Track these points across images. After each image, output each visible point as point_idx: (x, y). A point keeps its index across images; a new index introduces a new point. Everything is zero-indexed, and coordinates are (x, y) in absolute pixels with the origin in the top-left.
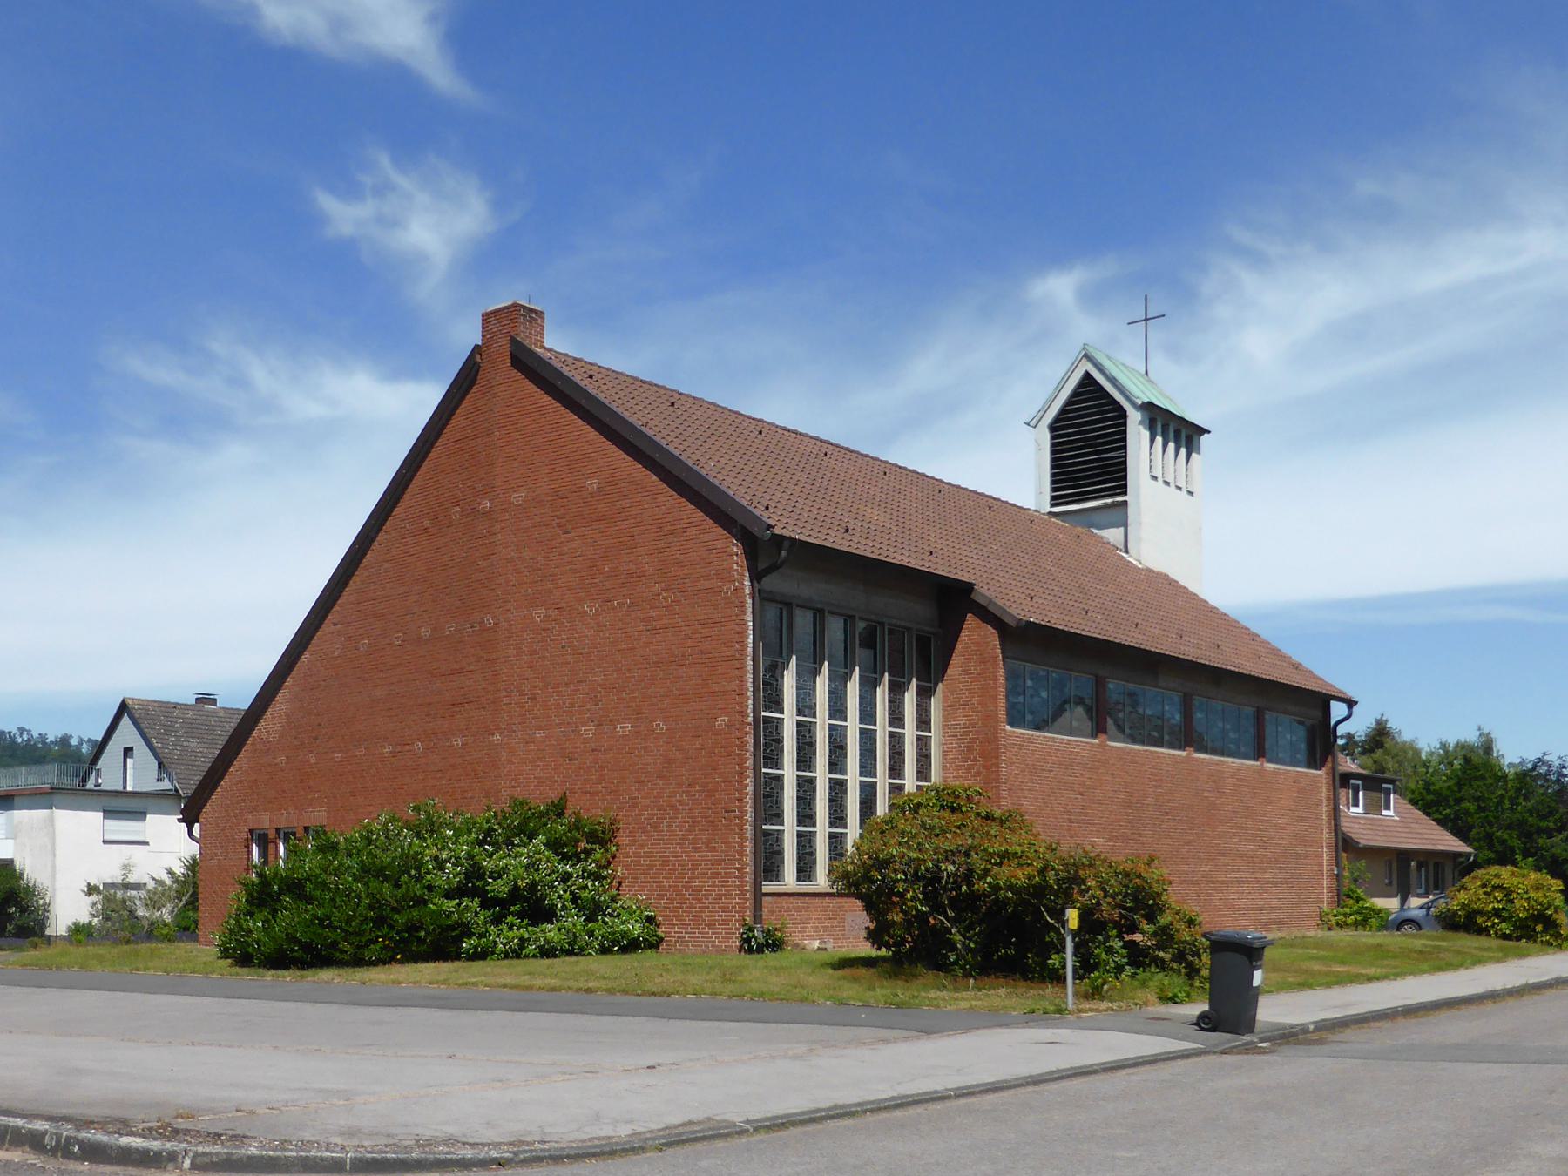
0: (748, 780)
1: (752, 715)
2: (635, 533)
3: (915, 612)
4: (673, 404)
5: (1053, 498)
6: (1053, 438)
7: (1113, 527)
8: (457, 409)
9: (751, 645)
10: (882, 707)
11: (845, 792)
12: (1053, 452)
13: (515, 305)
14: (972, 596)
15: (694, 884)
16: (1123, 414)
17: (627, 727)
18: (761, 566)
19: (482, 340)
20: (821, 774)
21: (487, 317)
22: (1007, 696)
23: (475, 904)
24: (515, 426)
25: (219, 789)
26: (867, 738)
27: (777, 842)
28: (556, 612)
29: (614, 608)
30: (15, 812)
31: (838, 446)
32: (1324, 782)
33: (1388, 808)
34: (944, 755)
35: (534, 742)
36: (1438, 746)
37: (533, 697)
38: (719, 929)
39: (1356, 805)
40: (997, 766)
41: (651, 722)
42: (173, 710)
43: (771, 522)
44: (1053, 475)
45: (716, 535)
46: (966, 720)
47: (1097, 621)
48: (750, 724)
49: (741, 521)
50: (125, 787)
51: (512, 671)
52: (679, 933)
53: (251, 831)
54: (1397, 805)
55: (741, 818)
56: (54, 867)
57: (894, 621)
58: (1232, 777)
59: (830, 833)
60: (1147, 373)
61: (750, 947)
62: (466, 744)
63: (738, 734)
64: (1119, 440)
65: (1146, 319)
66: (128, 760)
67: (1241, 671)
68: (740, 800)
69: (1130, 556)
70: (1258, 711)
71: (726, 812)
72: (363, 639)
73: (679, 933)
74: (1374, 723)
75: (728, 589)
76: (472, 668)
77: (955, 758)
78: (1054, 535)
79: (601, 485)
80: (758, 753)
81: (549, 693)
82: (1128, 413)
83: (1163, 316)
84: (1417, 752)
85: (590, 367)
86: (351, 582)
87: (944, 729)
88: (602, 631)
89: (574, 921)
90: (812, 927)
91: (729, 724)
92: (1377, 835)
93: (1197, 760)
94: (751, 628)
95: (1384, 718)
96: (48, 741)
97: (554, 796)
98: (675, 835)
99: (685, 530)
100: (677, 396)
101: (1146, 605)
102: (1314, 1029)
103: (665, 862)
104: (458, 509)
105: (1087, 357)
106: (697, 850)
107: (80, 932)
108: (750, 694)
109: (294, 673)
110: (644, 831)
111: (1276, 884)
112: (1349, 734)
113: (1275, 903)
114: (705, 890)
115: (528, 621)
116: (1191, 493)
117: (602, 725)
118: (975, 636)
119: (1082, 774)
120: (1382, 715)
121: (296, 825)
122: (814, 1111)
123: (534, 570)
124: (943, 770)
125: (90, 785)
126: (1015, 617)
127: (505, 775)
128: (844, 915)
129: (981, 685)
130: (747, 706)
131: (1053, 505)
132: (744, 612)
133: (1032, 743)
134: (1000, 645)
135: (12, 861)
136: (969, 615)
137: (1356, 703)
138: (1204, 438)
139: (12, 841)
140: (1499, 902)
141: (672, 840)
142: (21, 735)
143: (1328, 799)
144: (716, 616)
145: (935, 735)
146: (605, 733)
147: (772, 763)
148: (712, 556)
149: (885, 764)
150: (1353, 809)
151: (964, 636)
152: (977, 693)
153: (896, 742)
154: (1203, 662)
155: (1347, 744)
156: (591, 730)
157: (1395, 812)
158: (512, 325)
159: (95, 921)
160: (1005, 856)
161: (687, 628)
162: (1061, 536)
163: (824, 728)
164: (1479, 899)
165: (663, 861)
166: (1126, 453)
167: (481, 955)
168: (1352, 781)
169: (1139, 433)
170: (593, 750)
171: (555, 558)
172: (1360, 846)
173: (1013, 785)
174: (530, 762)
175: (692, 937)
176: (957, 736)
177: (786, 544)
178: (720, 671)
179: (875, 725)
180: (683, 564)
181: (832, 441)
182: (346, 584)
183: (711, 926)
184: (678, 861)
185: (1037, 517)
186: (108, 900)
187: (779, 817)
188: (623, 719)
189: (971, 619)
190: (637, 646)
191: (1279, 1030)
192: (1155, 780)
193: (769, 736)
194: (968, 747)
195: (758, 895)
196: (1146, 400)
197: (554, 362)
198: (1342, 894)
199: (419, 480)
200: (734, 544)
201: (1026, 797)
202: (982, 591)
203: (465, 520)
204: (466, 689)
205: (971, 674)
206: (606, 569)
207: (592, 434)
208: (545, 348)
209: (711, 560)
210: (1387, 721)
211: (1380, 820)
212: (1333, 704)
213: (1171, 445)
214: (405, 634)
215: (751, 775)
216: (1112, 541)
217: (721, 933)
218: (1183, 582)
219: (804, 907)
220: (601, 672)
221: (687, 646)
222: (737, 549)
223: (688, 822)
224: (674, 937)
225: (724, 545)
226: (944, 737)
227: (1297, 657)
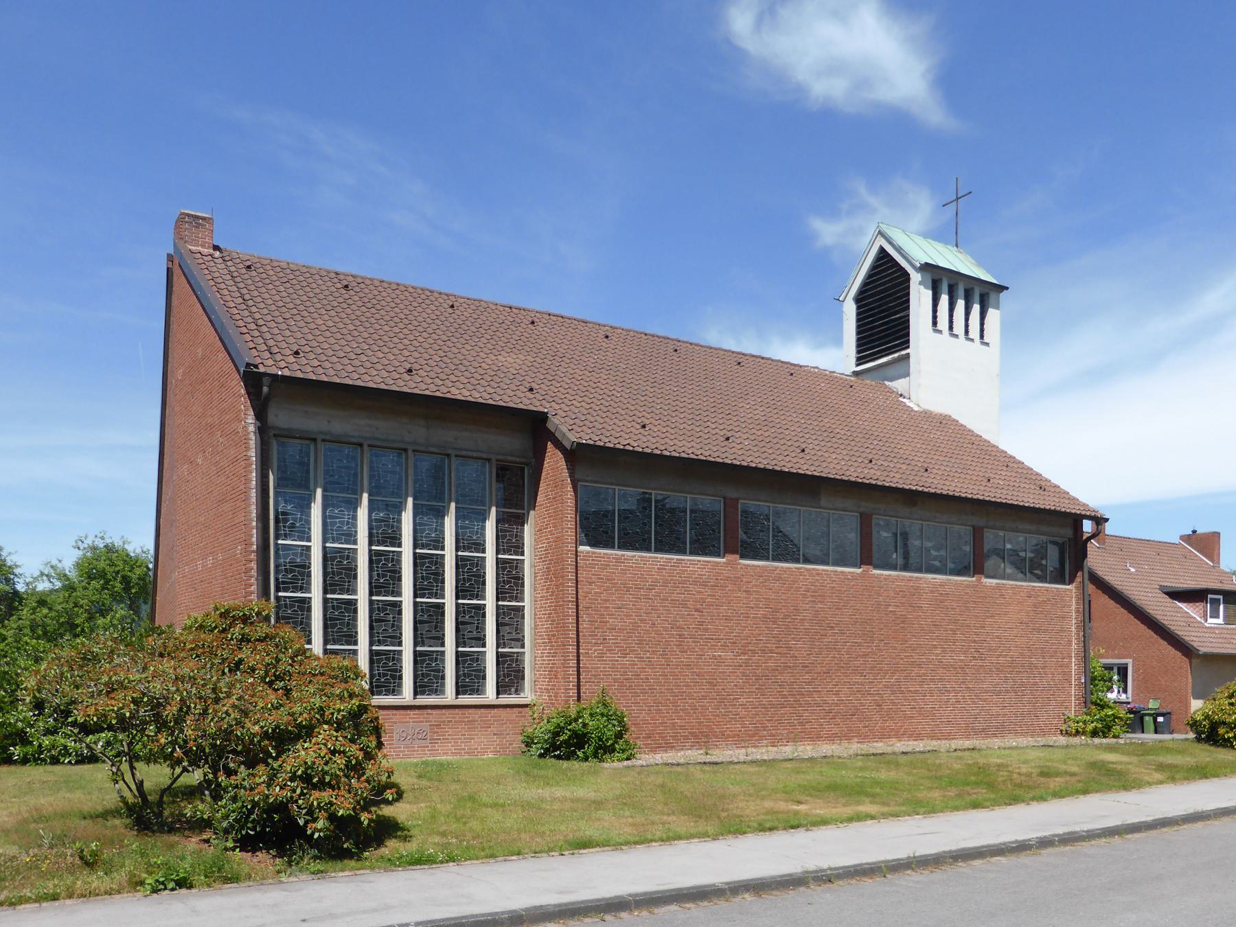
4: (739, 363)
5: (858, 359)
6: (858, 308)
44: (858, 340)
48: (253, 552)
58: (932, 592)
65: (958, 199)
93: (878, 577)
100: (351, 279)
105: (881, 233)
113: (995, 710)
131: (857, 365)
132: (247, 449)
137: (1107, 520)
143: (1077, 611)
151: (547, 460)
168: (1210, 596)
198: (1088, 702)
201: (612, 615)
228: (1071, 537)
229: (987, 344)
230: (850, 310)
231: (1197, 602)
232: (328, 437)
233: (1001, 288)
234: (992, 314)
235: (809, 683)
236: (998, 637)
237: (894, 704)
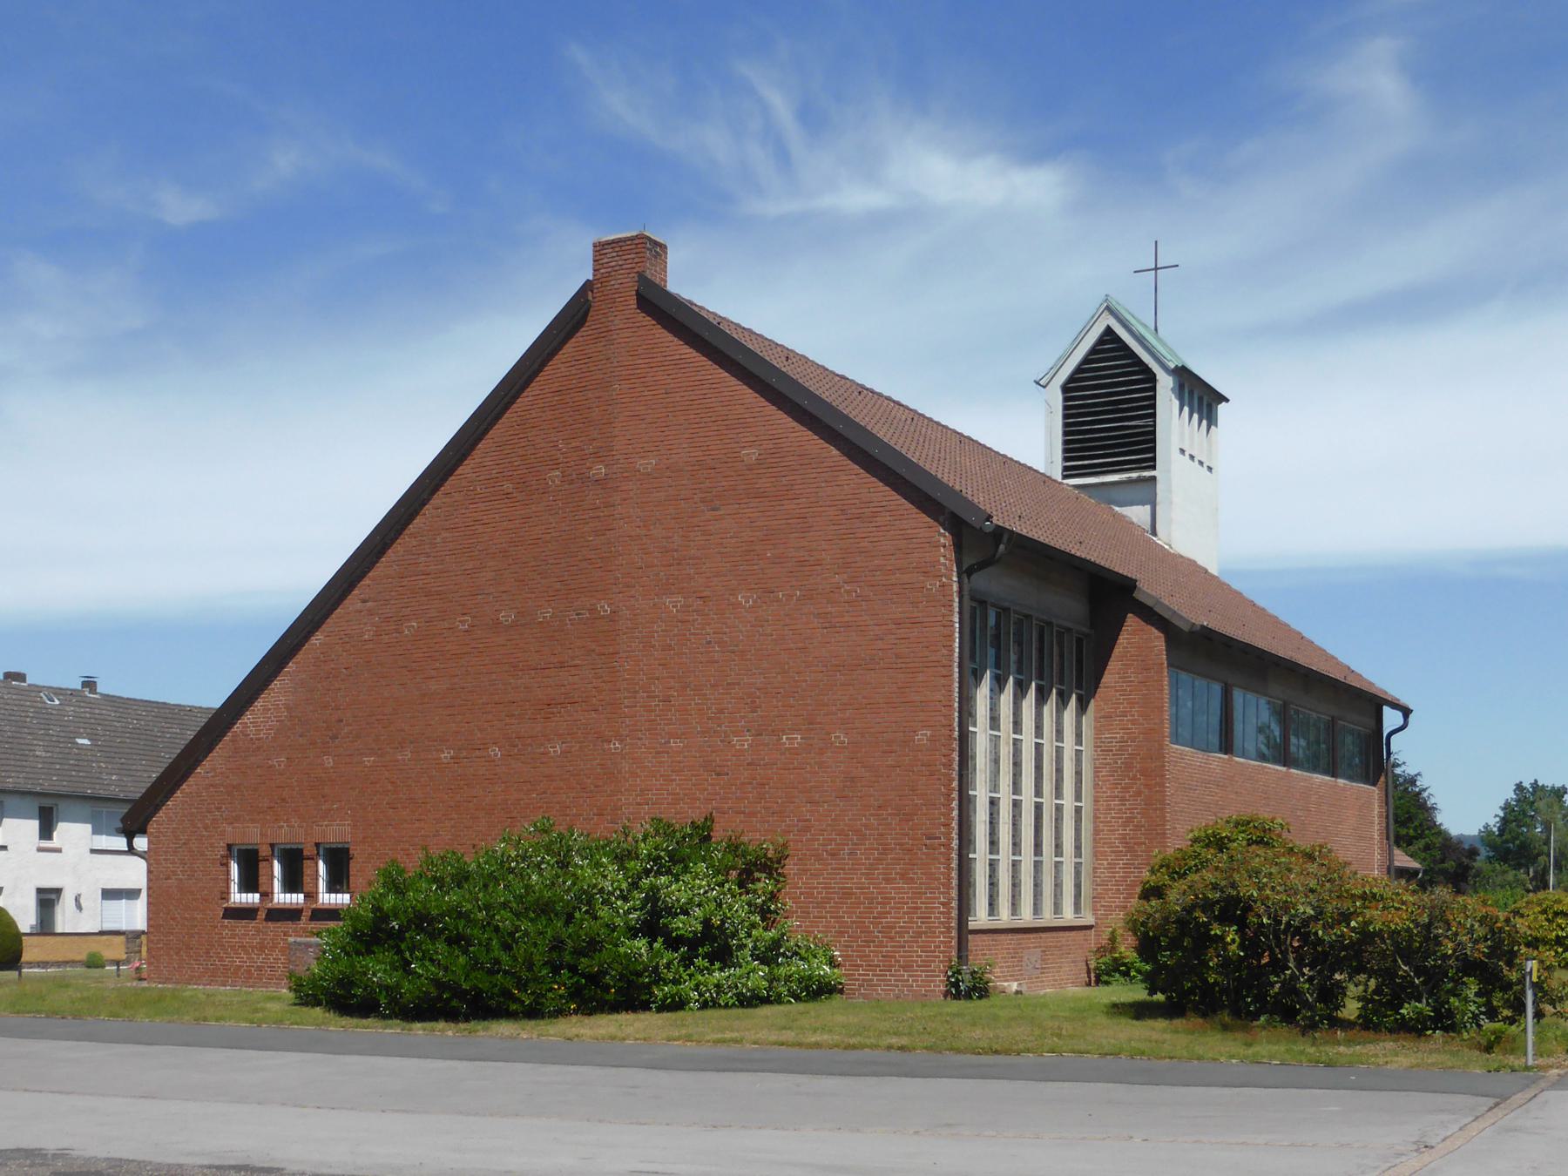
3: (1068, 608)
5: (1065, 469)
6: (1066, 399)
7: (1138, 504)
8: (556, 354)
10: (1049, 719)
12: (1065, 416)
14: (1134, 595)
15: (884, 920)
16: (1152, 378)
17: (796, 738)
19: (594, 275)
21: (600, 248)
24: (643, 380)
25: (178, 794)
28: (700, 602)
29: (778, 601)
32: (1377, 798)
34: (1095, 772)
35: (668, 753)
37: (667, 700)
38: (917, 971)
40: (1162, 785)
44: (1066, 442)
46: (1124, 733)
49: (951, 505)
51: (637, 668)
53: (229, 847)
60: (1156, 330)
61: (959, 992)
63: (944, 751)
65: (1156, 269)
69: (1159, 539)
70: (1333, 720)
72: (409, 620)
76: (577, 662)
79: (760, 457)
82: (1157, 378)
88: (762, 626)
91: (932, 740)
99: (875, 514)
103: (847, 894)
104: (557, 473)
106: (888, 881)
108: (956, 705)
109: (299, 657)
110: (819, 858)
115: (660, 611)
116: (1210, 469)
117: (761, 735)
118: (1135, 638)
119: (1216, 793)
124: (1094, 789)
128: (1022, 952)
129: (1143, 695)
130: (954, 719)
134: (1167, 651)
136: (1130, 615)
140: (1563, 929)
143: (1380, 816)
144: (916, 615)
148: (910, 546)
149: (1052, 783)
151: (1123, 639)
152: (1137, 703)
156: (747, 740)
161: (877, 628)
163: (1009, 743)
164: (1542, 926)
165: (843, 894)
166: (1155, 422)
167: (676, 1004)
169: (1171, 400)
171: (697, 538)
174: (661, 776)
176: (1112, 751)
178: (920, 679)
183: (907, 967)
184: (863, 893)
189: (1132, 621)
194: (1126, 763)
199: (496, 433)
200: (941, 535)
203: (567, 487)
204: (568, 687)
205: (1131, 681)
206: (769, 555)
207: (749, 395)
209: (909, 551)
212: (1387, 711)
213: (1196, 416)
215: (957, 798)
217: (921, 976)
220: (760, 674)
222: (945, 538)
223: (878, 850)
224: (858, 980)
226: (1096, 751)
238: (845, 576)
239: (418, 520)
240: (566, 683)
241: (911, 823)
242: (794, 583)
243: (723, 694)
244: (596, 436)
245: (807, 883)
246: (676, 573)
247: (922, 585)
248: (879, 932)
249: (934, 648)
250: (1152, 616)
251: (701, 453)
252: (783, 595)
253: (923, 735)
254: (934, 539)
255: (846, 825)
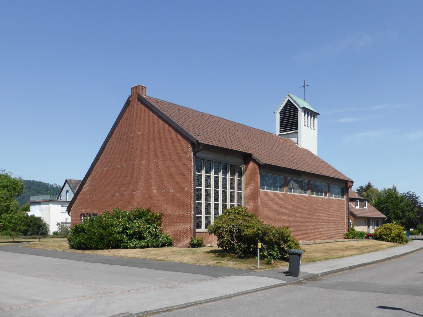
0: (192, 204)
1: (193, 188)
2: (166, 142)
4: (179, 109)
5: (280, 131)
6: (280, 116)
9: (193, 170)
11: (219, 206)
12: (280, 119)
13: (139, 85)
16: (297, 110)
18: (196, 150)
20: (212, 202)
22: (260, 182)
23: (125, 236)
26: (224, 193)
27: (200, 219)
30: (41, 206)
31: (223, 119)
33: (365, 206)
36: (383, 189)
39: (357, 206)
40: (257, 200)
41: (170, 189)
42: (77, 182)
43: (198, 139)
44: (280, 125)
45: (185, 142)
47: (285, 162)
48: (193, 190)
50: (67, 200)
52: (176, 242)
54: (368, 206)
55: (190, 213)
56: (50, 219)
57: (232, 164)
59: (214, 217)
62: (127, 194)
64: (296, 116)
65: (304, 86)
66: (68, 194)
67: (323, 175)
68: (190, 209)
71: (187, 212)
72: (105, 168)
73: (176, 242)
74: (367, 184)
75: (188, 156)
77: (247, 198)
78: (279, 140)
80: (195, 197)
81: (146, 182)
82: (299, 110)
83: (309, 85)
84: (378, 191)
85: (158, 100)
86: (102, 154)
87: (245, 190)
89: (149, 238)
90: (209, 240)
92: (362, 213)
94: (193, 166)
95: (370, 183)
96: (61, 187)
97: (147, 207)
98: (175, 217)
101: (300, 158)
102: (321, 275)
103: (173, 224)
105: (288, 95)
107: (55, 233)
108: (193, 182)
111: (332, 228)
112: (362, 186)
113: (332, 232)
114: (182, 231)
117: (158, 190)
119: (280, 201)
120: (370, 182)
121: (85, 213)
122: (157, 309)
123: (143, 151)
125: (59, 200)
126: (262, 162)
127: (136, 202)
131: (280, 133)
132: (191, 162)
133: (267, 194)
135: (41, 217)
137: (354, 182)
138: (318, 116)
139: (41, 212)
141: (175, 219)
142: (55, 185)
143: (346, 206)
145: (243, 192)
146: (159, 192)
147: (199, 200)
148: (184, 148)
150: (356, 207)
153: (232, 194)
154: (313, 173)
155: (361, 189)
157: (367, 207)
158: (138, 90)
159: (59, 232)
160: (248, 227)
162: (280, 140)
163: (213, 191)
165: (172, 224)
166: (298, 120)
170: (156, 196)
172: (358, 216)
173: (262, 204)
175: (179, 243)
177: (202, 145)
179: (227, 189)
180: (177, 150)
181: (222, 118)
182: (101, 154)
183: (183, 240)
185: (275, 136)
186: (62, 226)
187: (201, 213)
188: (163, 188)
190: (167, 170)
191: (313, 275)
192: (300, 202)
193: (198, 193)
195: (195, 233)
196: (303, 106)
197: (148, 100)
202: (254, 156)
207: (156, 117)
208: (147, 96)
209: (183, 149)
210: (371, 183)
211: (363, 210)
212: (348, 183)
213: (310, 116)
214: (114, 167)
215: (193, 203)
216: (294, 141)
218: (312, 152)
219: (207, 235)
221: (178, 170)
225: (187, 145)
227: (340, 170)
228: (345, 186)
229: (315, 129)
230: (278, 116)
231: (353, 201)
232: (207, 159)
233: (318, 114)
234: (316, 119)
235: (299, 225)
236: (332, 213)
237: (314, 231)
238: (172, 155)
239: (106, 147)
240: (127, 180)
241: (184, 208)
242: (164, 157)
243: (152, 181)
244: (131, 128)
245: (166, 222)
246: (144, 156)
247: (186, 156)
248: (178, 232)
249: (188, 170)
250: (255, 161)
251: (148, 130)
252: (162, 160)
253: (186, 189)
254: (188, 146)
255: (173, 209)
